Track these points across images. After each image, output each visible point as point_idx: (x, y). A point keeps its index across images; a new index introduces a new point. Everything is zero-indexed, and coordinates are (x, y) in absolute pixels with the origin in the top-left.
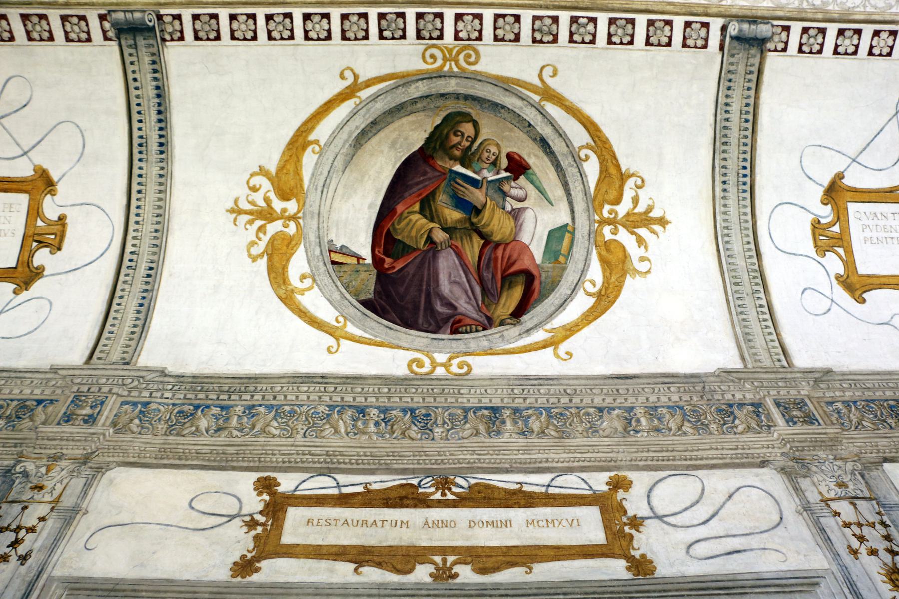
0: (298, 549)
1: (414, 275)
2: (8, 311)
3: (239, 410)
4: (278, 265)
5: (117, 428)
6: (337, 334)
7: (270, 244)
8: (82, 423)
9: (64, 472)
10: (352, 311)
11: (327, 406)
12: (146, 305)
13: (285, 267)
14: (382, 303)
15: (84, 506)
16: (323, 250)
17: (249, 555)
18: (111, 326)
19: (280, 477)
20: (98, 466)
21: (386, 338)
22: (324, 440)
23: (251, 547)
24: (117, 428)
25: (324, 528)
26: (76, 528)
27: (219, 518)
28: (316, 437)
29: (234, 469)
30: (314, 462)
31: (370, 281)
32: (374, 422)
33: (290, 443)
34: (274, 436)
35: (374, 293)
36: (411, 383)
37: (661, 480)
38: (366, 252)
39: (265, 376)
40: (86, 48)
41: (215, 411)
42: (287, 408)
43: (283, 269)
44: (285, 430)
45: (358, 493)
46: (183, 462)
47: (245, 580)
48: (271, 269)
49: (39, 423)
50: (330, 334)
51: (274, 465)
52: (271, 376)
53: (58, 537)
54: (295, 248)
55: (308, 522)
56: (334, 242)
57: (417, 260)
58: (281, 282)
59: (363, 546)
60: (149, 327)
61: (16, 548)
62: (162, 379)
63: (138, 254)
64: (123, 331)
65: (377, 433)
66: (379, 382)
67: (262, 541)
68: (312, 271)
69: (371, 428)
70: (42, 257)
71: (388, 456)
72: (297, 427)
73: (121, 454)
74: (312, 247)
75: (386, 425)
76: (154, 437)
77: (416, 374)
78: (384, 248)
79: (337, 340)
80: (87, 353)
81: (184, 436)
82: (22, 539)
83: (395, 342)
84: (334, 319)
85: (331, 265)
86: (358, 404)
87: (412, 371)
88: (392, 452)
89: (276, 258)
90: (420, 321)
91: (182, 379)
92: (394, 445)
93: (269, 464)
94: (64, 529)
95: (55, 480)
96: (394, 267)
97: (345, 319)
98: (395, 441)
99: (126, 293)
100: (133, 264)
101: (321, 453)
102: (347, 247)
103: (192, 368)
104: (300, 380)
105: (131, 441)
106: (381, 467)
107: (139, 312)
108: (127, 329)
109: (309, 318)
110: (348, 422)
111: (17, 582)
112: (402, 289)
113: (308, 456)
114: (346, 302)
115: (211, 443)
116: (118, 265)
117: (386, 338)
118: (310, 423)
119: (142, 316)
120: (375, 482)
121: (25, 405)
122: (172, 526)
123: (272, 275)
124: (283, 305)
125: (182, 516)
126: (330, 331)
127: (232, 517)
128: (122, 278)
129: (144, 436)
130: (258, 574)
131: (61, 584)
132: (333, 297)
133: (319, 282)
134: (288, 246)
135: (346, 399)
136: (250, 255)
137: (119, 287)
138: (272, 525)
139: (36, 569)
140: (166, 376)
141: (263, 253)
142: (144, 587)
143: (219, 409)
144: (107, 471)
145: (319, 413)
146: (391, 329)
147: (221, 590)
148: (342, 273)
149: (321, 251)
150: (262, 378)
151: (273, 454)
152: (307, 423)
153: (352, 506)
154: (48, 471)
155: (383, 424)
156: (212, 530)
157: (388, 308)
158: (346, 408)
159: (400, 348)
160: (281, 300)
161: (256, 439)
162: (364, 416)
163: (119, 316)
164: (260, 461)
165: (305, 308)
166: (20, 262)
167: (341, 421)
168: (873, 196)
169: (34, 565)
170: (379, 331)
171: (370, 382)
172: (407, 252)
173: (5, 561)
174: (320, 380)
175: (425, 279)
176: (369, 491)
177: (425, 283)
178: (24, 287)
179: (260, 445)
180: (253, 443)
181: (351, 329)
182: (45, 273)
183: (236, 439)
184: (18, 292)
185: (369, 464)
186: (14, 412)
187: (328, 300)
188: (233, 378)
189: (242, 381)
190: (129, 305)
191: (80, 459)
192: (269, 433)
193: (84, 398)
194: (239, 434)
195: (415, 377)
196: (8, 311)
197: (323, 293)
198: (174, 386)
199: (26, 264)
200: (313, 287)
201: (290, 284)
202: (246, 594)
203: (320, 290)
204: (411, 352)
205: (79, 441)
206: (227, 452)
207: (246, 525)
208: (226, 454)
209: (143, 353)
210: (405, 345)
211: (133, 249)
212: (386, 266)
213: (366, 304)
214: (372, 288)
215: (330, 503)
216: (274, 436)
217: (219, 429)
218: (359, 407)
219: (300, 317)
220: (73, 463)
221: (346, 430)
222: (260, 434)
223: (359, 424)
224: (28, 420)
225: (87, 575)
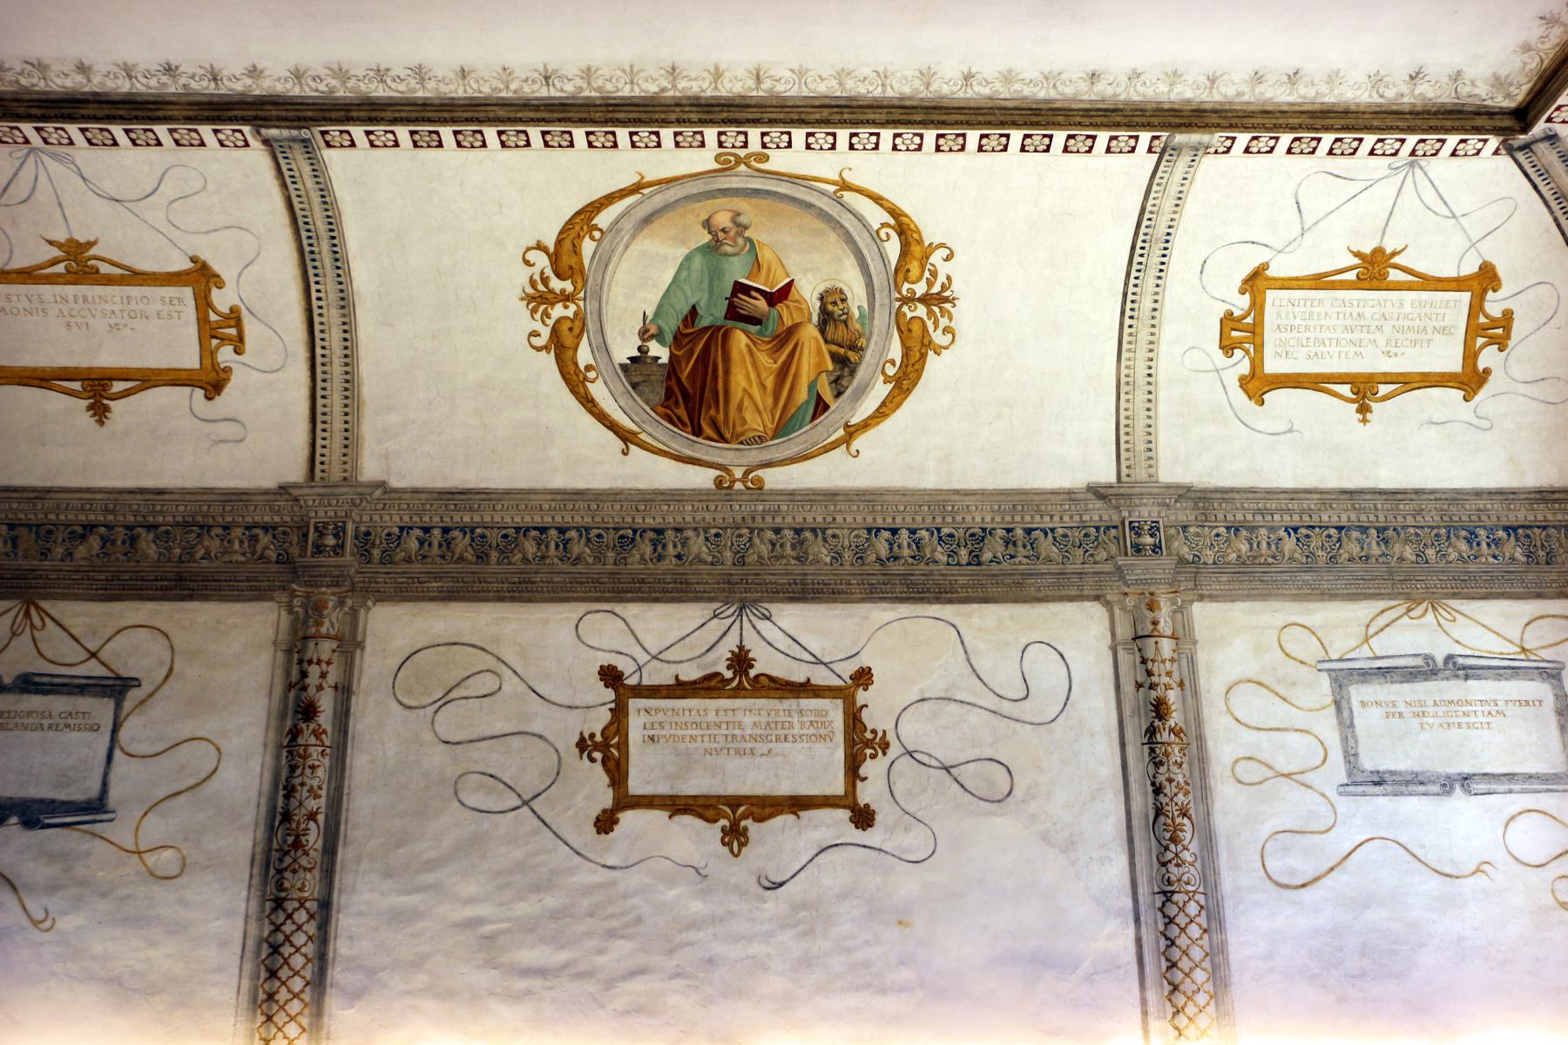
37: (1354, 649)
40: (482, 152)
70: (1488, 358)
168: (1446, 285)
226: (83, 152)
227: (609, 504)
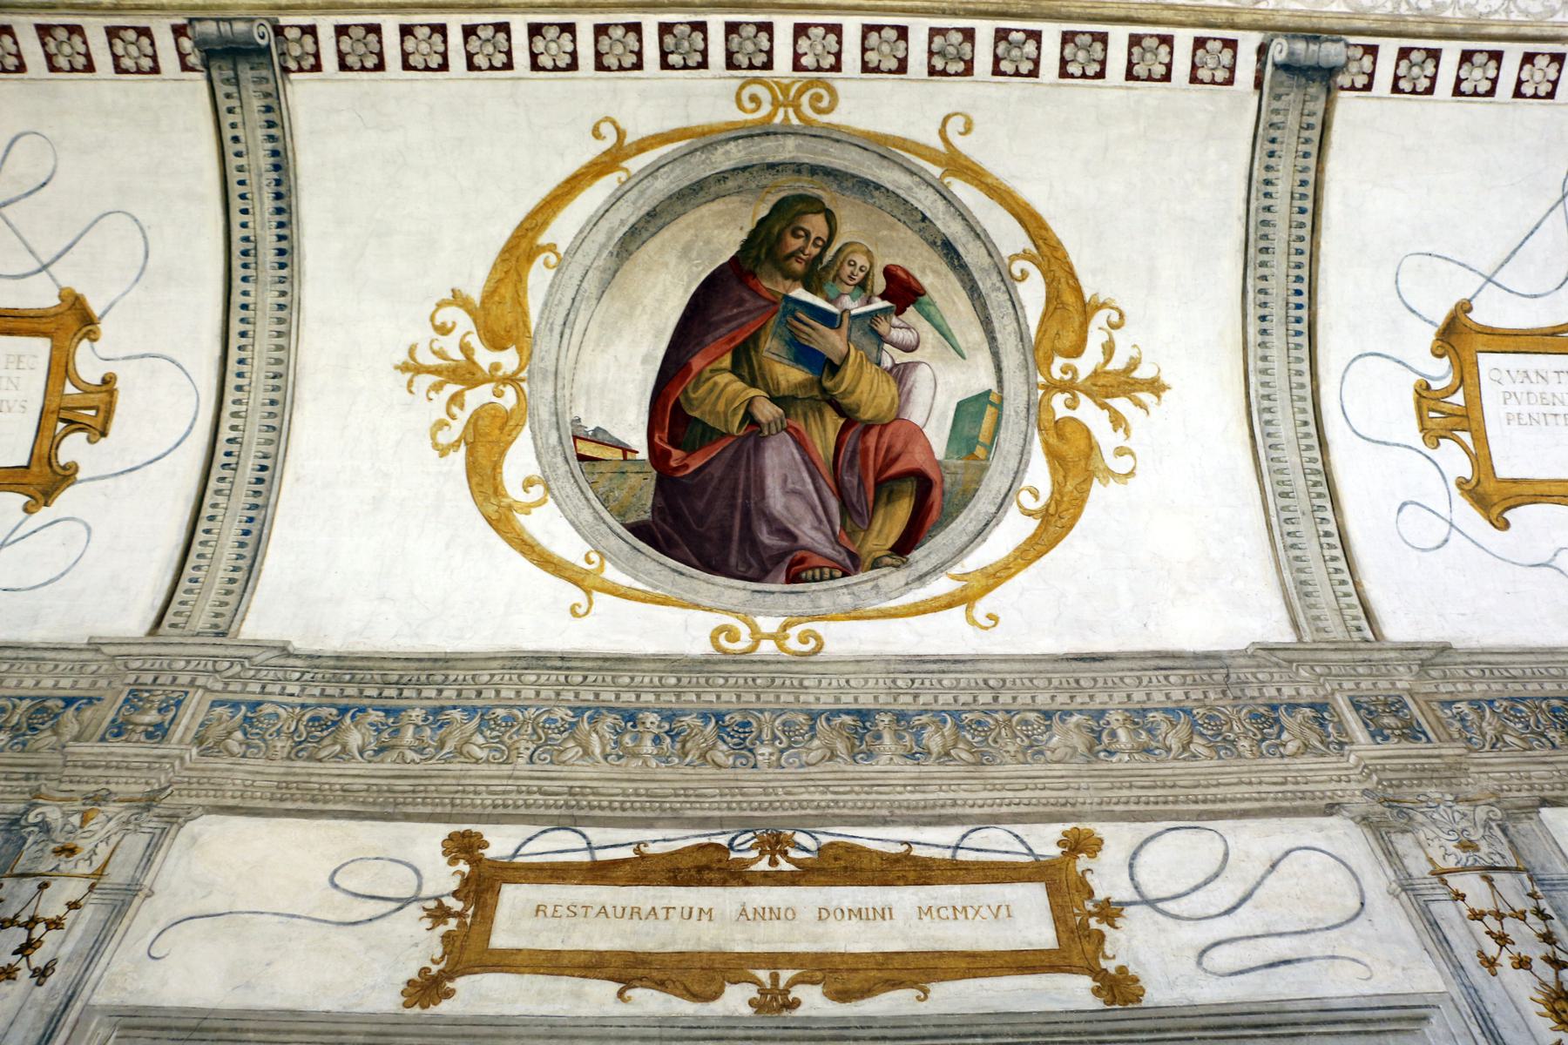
0: (519, 958)
1: (721, 480)
2: (14, 542)
3: (417, 715)
4: (484, 462)
5: (203, 747)
6: (589, 582)
7: (471, 426)
8: (143, 738)
9: (112, 823)
10: (614, 542)
11: (570, 708)
12: (255, 533)
13: (496, 467)
14: (667, 528)
15: (147, 882)
16: (564, 437)
17: (435, 969)
18: (194, 568)
19: (489, 832)
20: (170, 812)
21: (674, 590)
22: (566, 768)
23: (438, 955)
24: (203, 747)
25: (565, 921)
26: (132, 920)
27: (381, 903)
28: (552, 762)
29: (408, 817)
30: (548, 807)
31: (645, 490)
32: (652, 736)
33: (506, 773)
34: (477, 761)
35: (653, 512)
36: (717, 668)
37: (1152, 838)
38: (638, 440)
39: (463, 657)
40: (149, 84)
41: (375, 716)
42: (501, 712)
43: (494, 469)
44: (496, 750)
45: (625, 861)
46: (319, 806)
47: (427, 1011)
48: (472, 469)
49: (68, 737)
50: (576, 583)
51: (478, 811)
52: (473, 656)
53: (102, 937)
54: (514, 433)
55: (538, 911)
56: (583, 423)
57: (728, 454)
58: (490, 492)
59: (633, 953)
60: (260, 571)
61: (27, 956)
62: (282, 662)
63: (241, 444)
64: (215, 578)
65: (657, 756)
66: (661, 666)
67: (458, 944)
68: (543, 472)
69: (648, 746)
70: (73, 448)
71: (677, 795)
72: (517, 745)
73: (212, 793)
74: (544, 430)
75: (673, 741)
76: (269, 763)
77: (725, 652)
78: (669, 433)
79: (588, 592)
80: (152, 616)
81: (320, 760)
82: (39, 940)
83: (689, 597)
84: (583, 557)
85: (577, 463)
86: (624, 705)
87: (718, 648)
88: (684, 789)
89: (481, 450)
90: (733, 560)
91: (317, 662)
92: (688, 777)
93: (469, 810)
94: (112, 924)
95: (97, 837)
96: (686, 466)
97: (602, 556)
98: (689, 770)
99: (219, 512)
100: (232, 460)
101: (560, 789)
102: (605, 432)
103: (334, 642)
104: (523, 663)
105: (228, 770)
106: (664, 815)
107: (242, 545)
108: (221, 574)
109: (538, 554)
110: (607, 735)
111: (30, 1016)
112: (700, 505)
113: (537, 796)
114: (604, 526)
115: (367, 773)
116: (205, 462)
117: (674, 590)
118: (540, 739)
119: (248, 552)
120: (655, 841)
121: (44, 707)
122: (299, 917)
123: (475, 480)
124: (493, 533)
125: (317, 899)
126: (575, 577)
127: (404, 903)
128: (213, 484)
129: (252, 761)
130: (450, 1001)
131: (107, 1020)
132: (581, 518)
133: (556, 492)
134: (501, 429)
135: (603, 696)
136: (435, 446)
137: (208, 500)
138: (474, 915)
139: (63, 992)
140: (289, 655)
141: (459, 441)
142: (251, 1025)
143: (382, 714)
144: (186, 821)
145: (556, 721)
146: (681, 574)
147: (385, 1028)
148: (596, 476)
149: (560, 438)
150: (456, 660)
151: (475, 793)
152: (535, 737)
153: (614, 882)
154: (84, 821)
155: (668, 740)
156: (370, 924)
157: (676, 537)
158: (604, 711)
159: (697, 606)
160: (491, 524)
161: (447, 766)
162: (634, 726)
163: (208, 551)
164: (453, 805)
165: (531, 537)
166: (35, 457)
167: (594, 735)
168: (1523, 342)
169: (59, 985)
170: (662, 578)
171: (645, 666)
172: (710, 439)
173: (8, 978)
174: (559, 664)
175: (741, 487)
176: (643, 857)
177: (741, 493)
178: (42, 502)
179: (454, 777)
180: (442, 773)
181: (612, 574)
182: (79, 476)
183: (412, 766)
184: (31, 509)
185: (643, 809)
186: (24, 719)
187: (572, 523)
188: (407, 659)
189: (423, 665)
190: (225, 532)
191: (140, 800)
192: (470, 755)
193: (146, 695)
194: (417, 757)
195: (723, 657)
196: (14, 542)
197: (563, 511)
198: (303, 673)
199: (45, 460)
200: (545, 501)
201: (506, 496)
202: (429, 1036)
203: (559, 505)
204: (717, 615)
205: (137, 769)
206: (396, 788)
207: (429, 916)
208: (394, 792)
209: (249, 617)
210: (707, 602)
211: (233, 434)
212: (673, 464)
213: (639, 530)
214: (649, 503)
215: (575, 878)
216: (477, 761)
217: (382, 749)
218: (626, 710)
219: (523, 553)
220: (127, 808)
221: (603, 751)
222: (454, 757)
223: (627, 739)
224: (48, 733)
225: (152, 1003)
226: (853, 85)
227: (1207, 702)
